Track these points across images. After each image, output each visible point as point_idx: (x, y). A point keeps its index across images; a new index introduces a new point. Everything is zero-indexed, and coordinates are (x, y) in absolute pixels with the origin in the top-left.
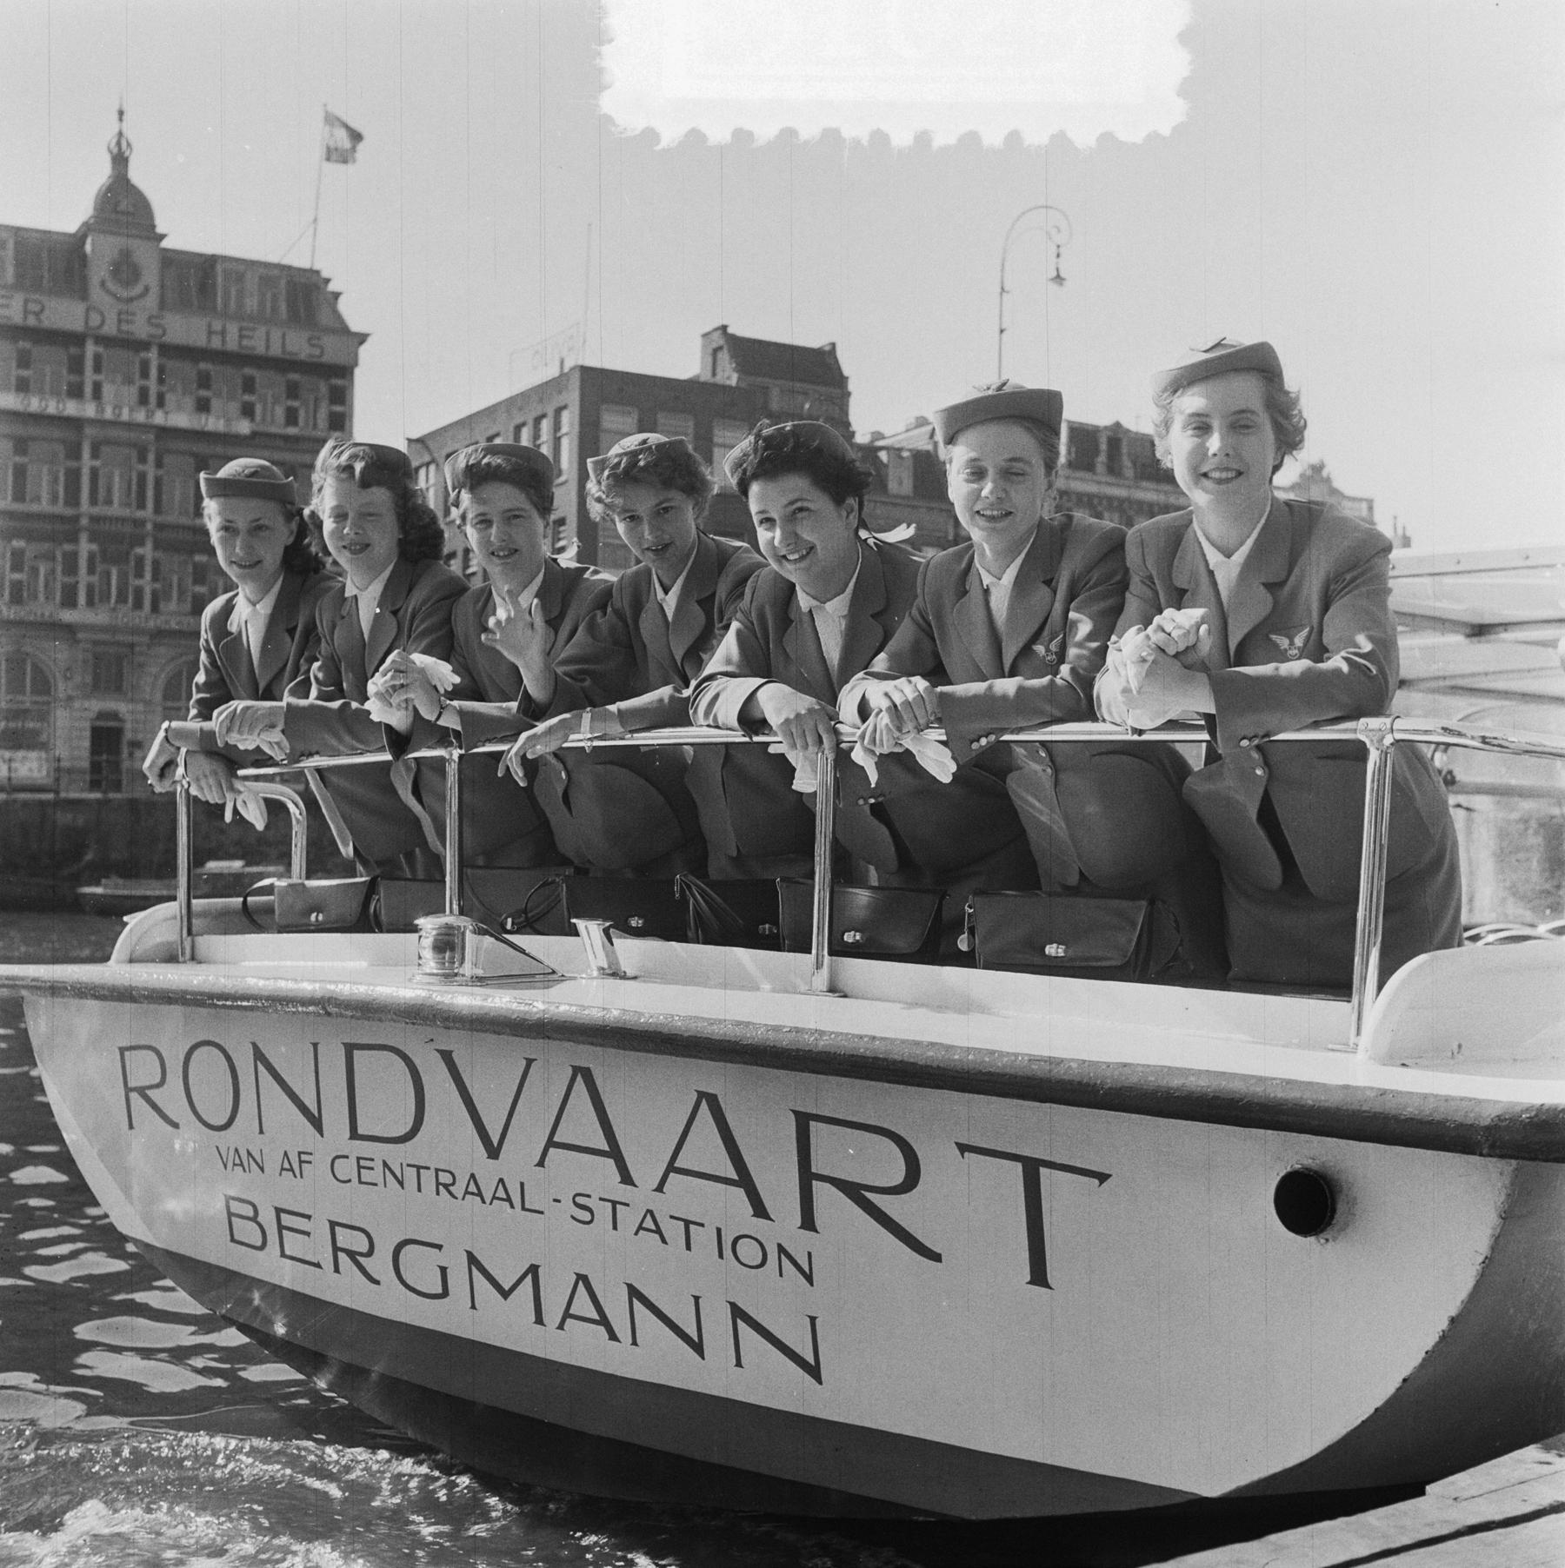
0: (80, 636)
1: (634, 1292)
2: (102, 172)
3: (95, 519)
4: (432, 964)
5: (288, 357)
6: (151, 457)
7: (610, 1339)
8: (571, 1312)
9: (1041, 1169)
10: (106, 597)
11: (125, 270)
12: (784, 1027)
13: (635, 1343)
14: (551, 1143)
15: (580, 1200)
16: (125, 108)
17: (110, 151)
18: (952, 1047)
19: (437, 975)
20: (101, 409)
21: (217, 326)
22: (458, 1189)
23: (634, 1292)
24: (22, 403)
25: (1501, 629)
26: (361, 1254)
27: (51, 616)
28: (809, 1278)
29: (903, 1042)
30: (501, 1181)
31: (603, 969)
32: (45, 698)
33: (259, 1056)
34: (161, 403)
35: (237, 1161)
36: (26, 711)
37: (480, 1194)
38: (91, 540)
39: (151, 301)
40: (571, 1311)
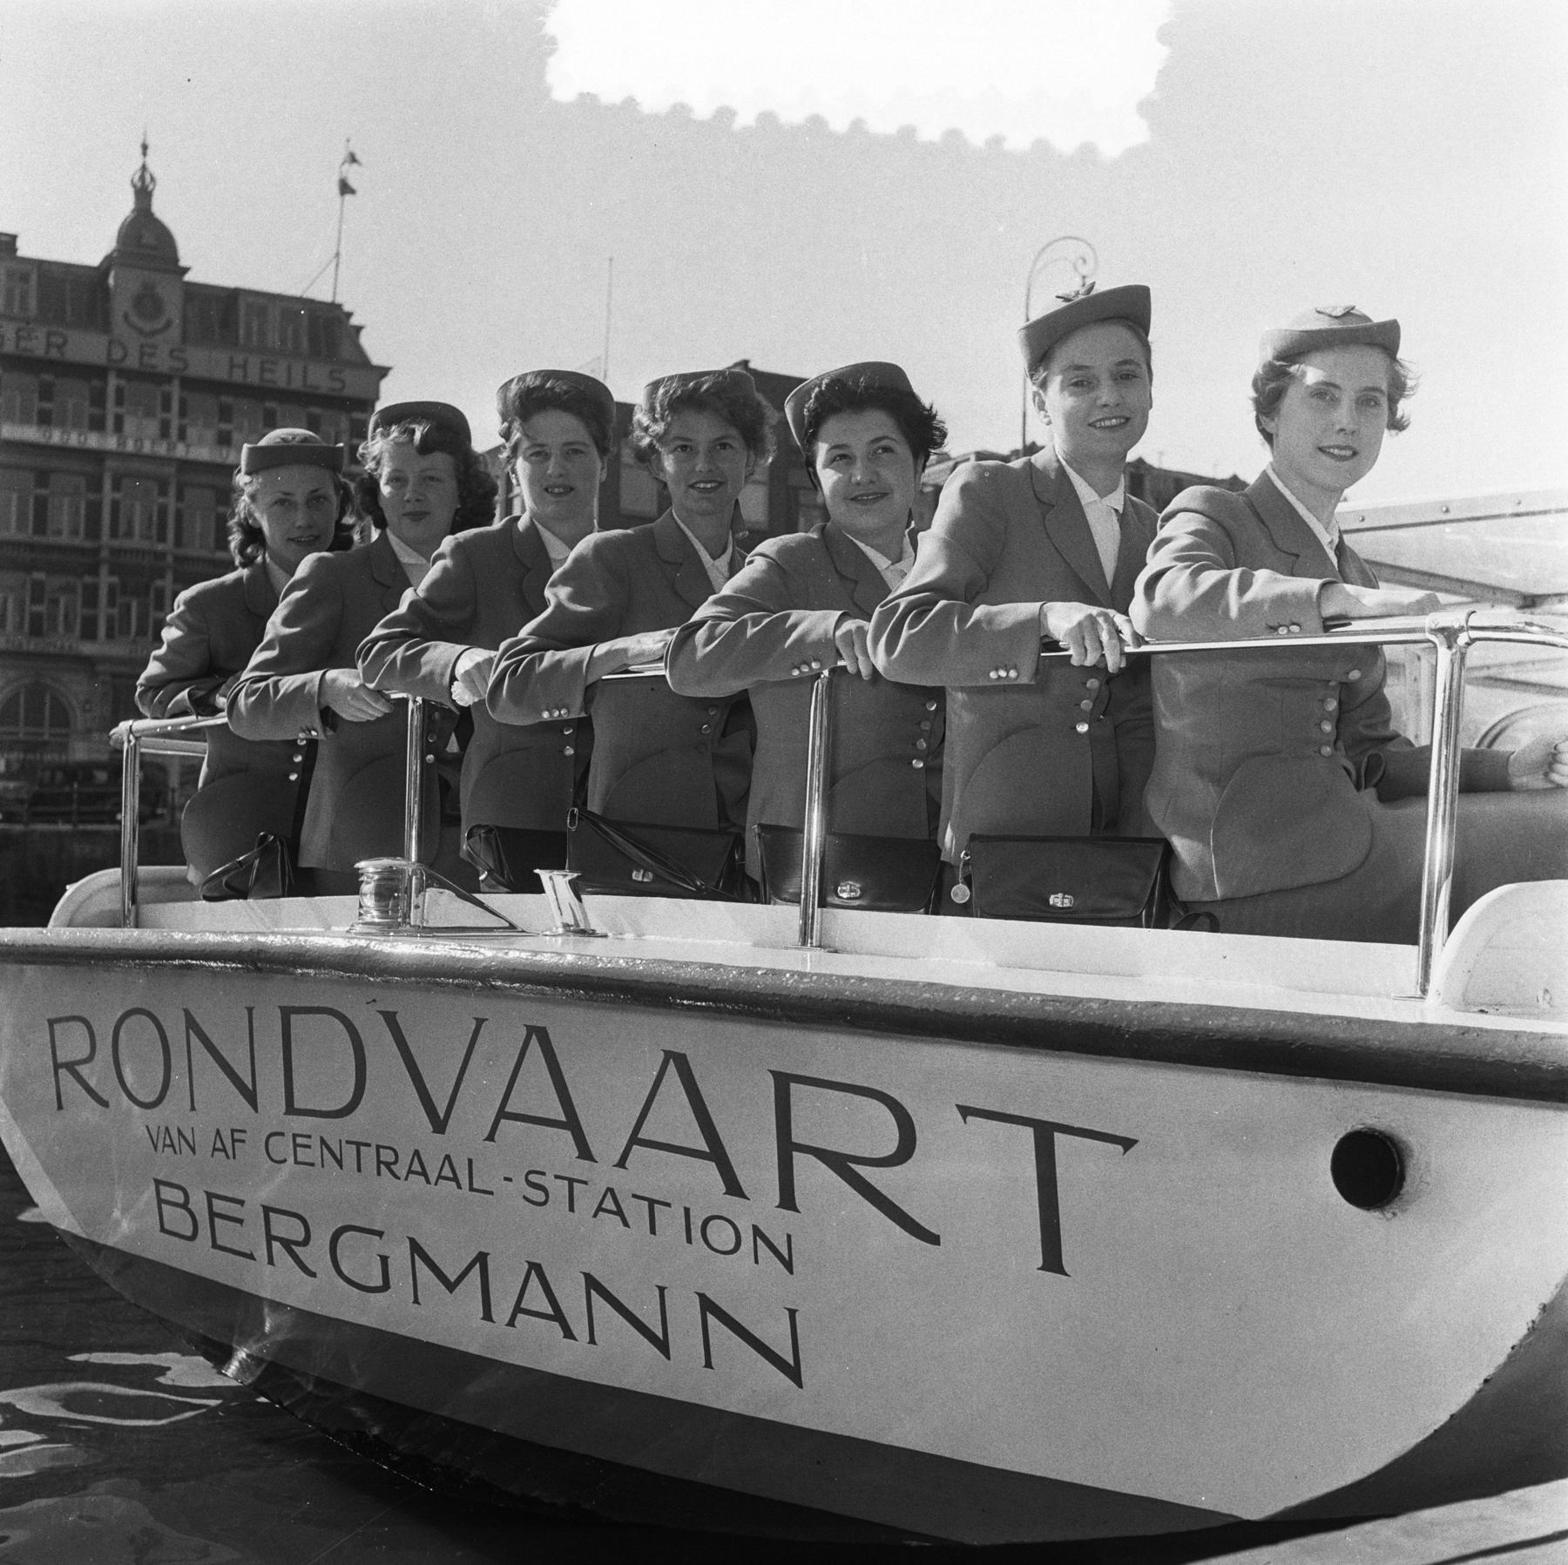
0: (100, 668)
1: (592, 1283)
2: (125, 205)
3: (116, 552)
4: (375, 913)
5: (308, 390)
6: (172, 490)
7: (565, 1337)
8: (523, 1306)
9: (1056, 1134)
10: (125, 631)
11: (148, 303)
12: (759, 969)
13: (592, 1341)
14: (502, 1114)
15: (533, 1178)
16: (151, 142)
17: (134, 186)
18: (952, 987)
19: (378, 924)
20: (122, 443)
21: (239, 359)
22: (401, 1169)
23: (592, 1283)
24: (44, 435)
25: (1555, 599)
26: (298, 1244)
27: (70, 647)
28: (789, 1265)
29: (895, 983)
30: (447, 1157)
31: (568, 926)
32: (64, 731)
33: (191, 1024)
34: (182, 436)
35: (168, 1142)
36: (45, 743)
37: (424, 1173)
38: (112, 572)
39: (175, 332)
40: (523, 1306)
